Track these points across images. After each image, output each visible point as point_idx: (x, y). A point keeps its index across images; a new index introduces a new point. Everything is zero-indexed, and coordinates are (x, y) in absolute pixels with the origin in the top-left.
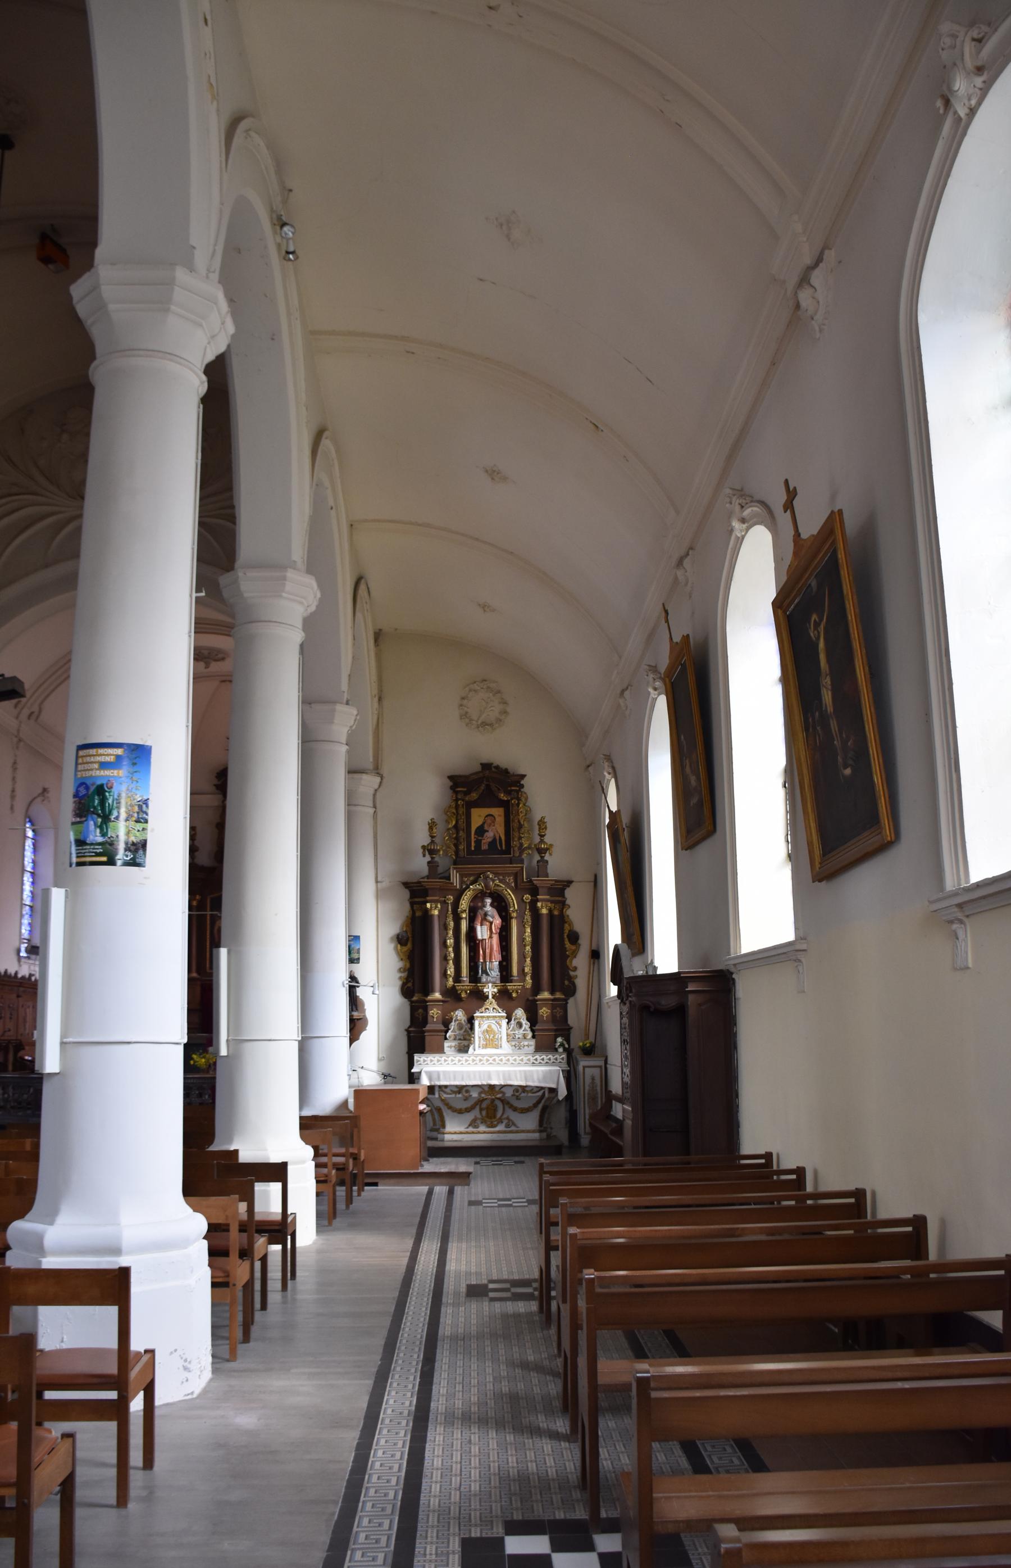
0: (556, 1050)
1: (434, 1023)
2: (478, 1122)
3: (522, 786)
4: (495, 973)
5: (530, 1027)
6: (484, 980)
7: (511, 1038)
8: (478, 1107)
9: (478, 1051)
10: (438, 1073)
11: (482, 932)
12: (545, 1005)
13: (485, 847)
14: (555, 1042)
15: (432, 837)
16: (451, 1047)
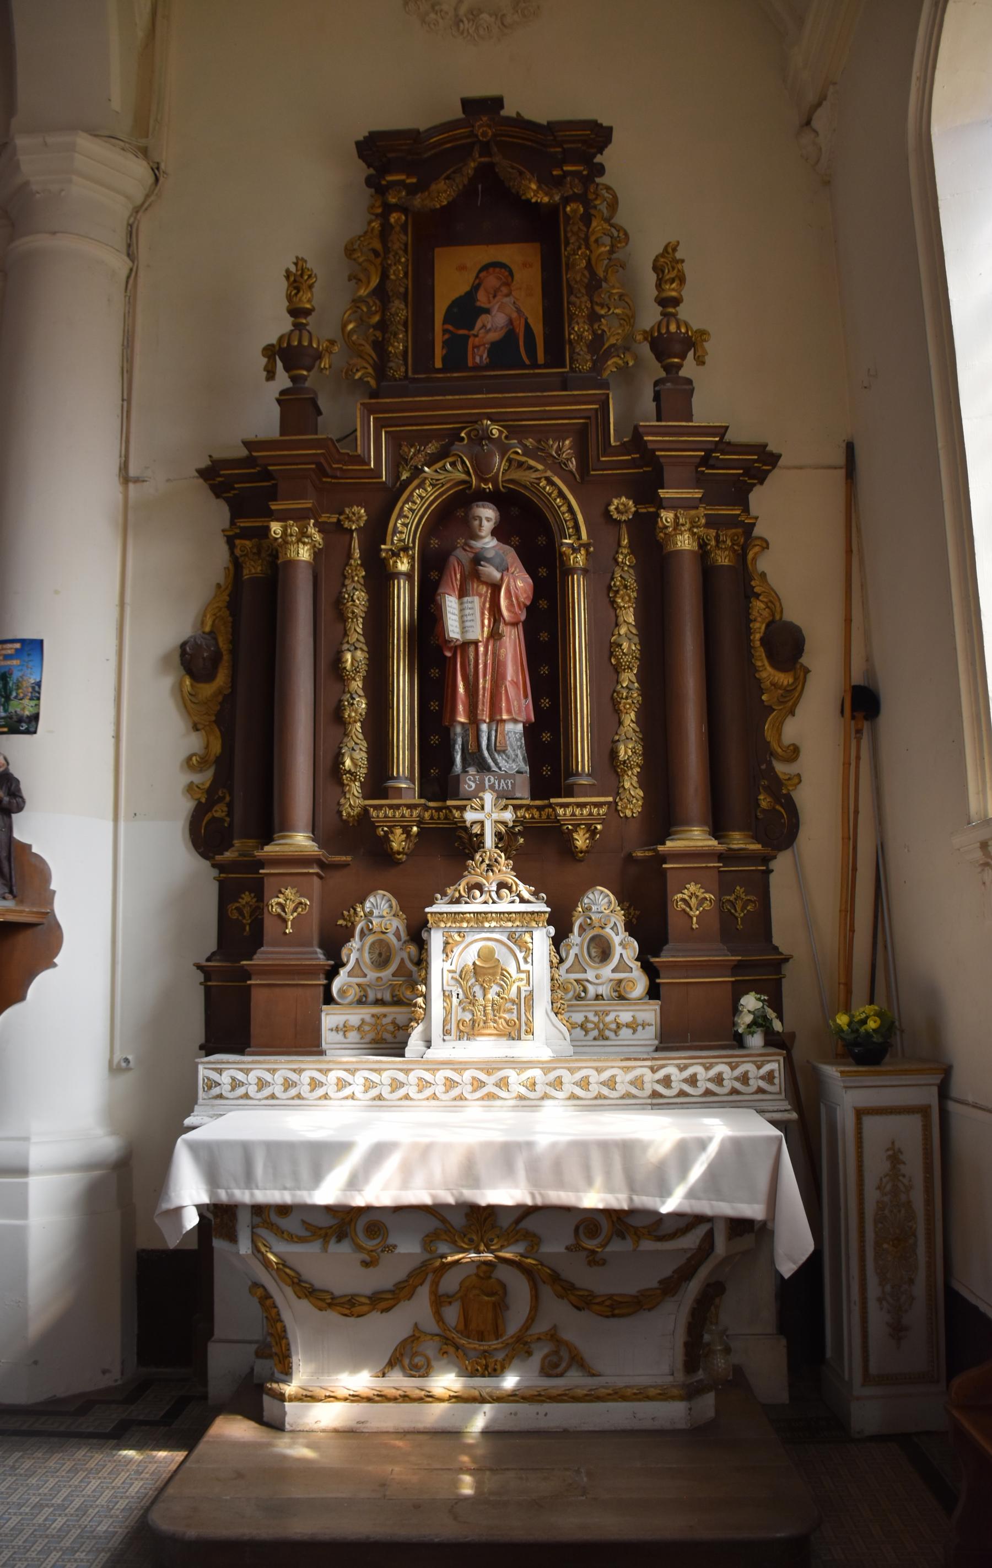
0: (739, 1041)
2: (429, 1348)
3: (600, 170)
4: (512, 761)
5: (642, 958)
6: (469, 783)
7: (567, 997)
8: (424, 1293)
9: (441, 1051)
10: (246, 1150)
11: (461, 618)
13: (479, 357)
14: (736, 1009)
15: (295, 312)
16: (344, 1029)
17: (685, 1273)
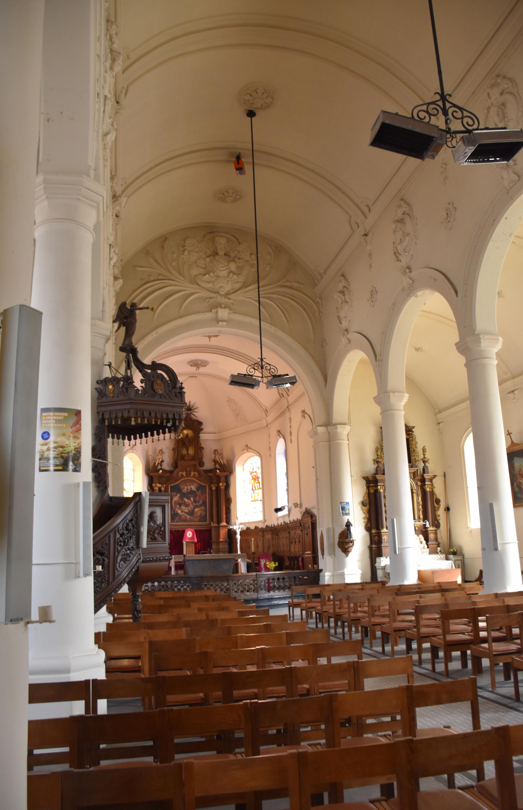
12: (432, 533)
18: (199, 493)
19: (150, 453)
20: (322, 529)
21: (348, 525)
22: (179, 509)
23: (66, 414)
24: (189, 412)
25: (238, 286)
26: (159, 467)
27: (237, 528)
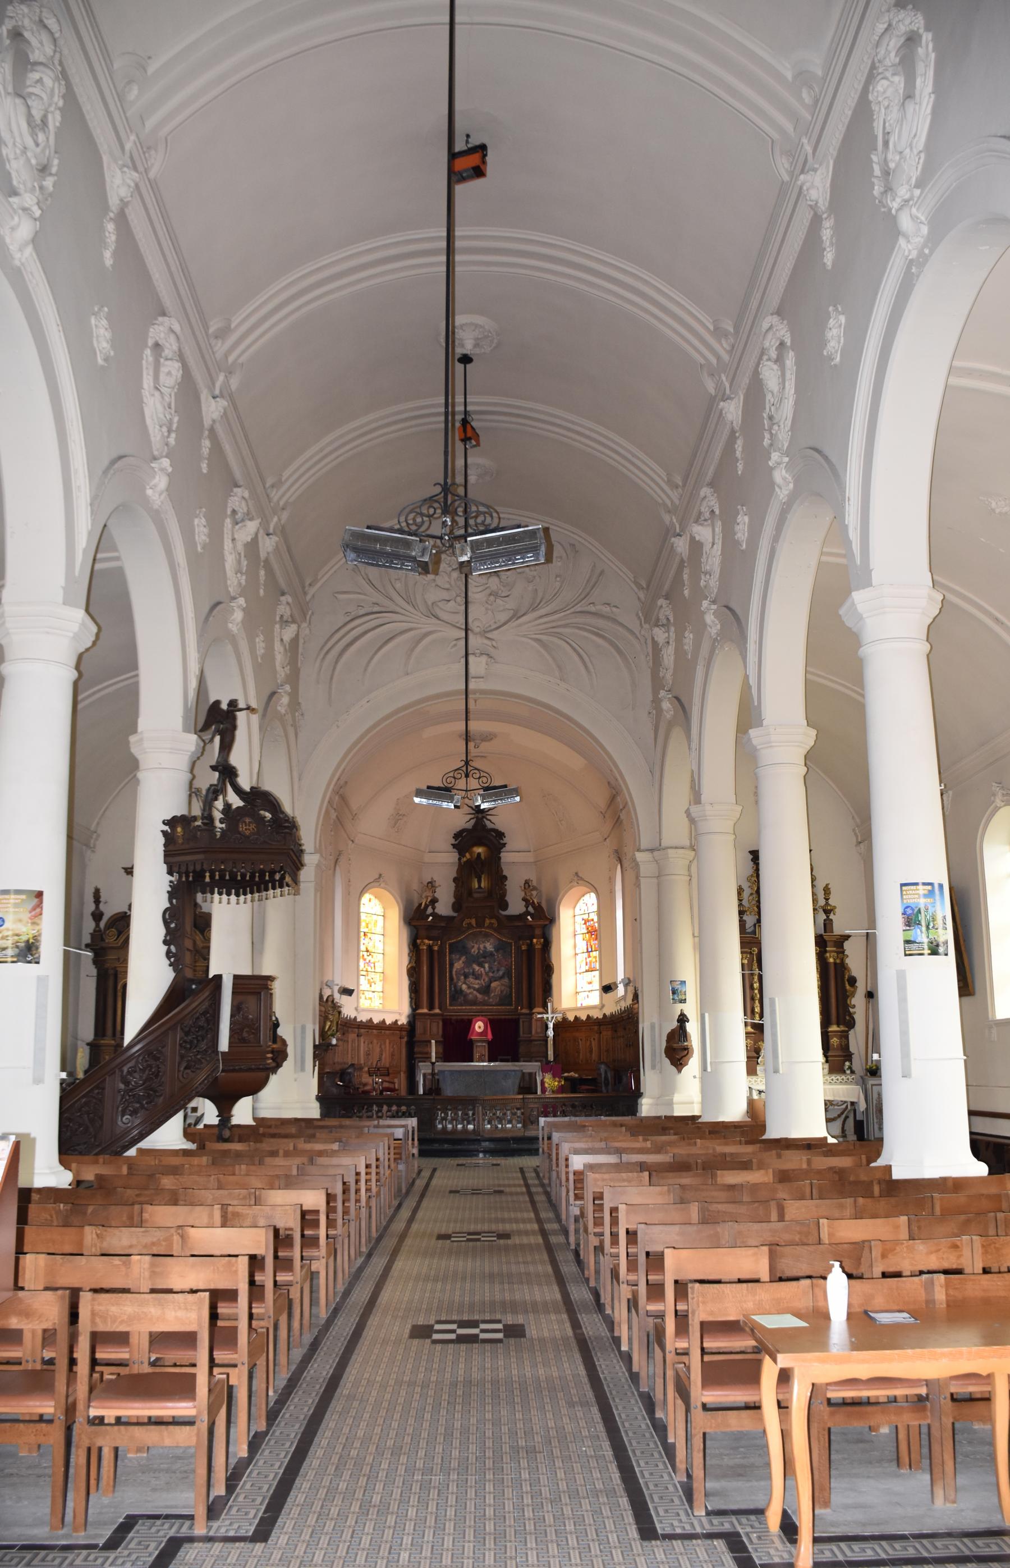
1: (834, 1049)
12: (835, 1036)
17: (842, 1113)
18: (499, 956)
19: (415, 886)
20: (645, 1026)
21: (683, 1019)
22: (465, 983)
23: (24, 897)
24: (480, 816)
25: (503, 617)
26: (430, 910)
27: (551, 1019)
